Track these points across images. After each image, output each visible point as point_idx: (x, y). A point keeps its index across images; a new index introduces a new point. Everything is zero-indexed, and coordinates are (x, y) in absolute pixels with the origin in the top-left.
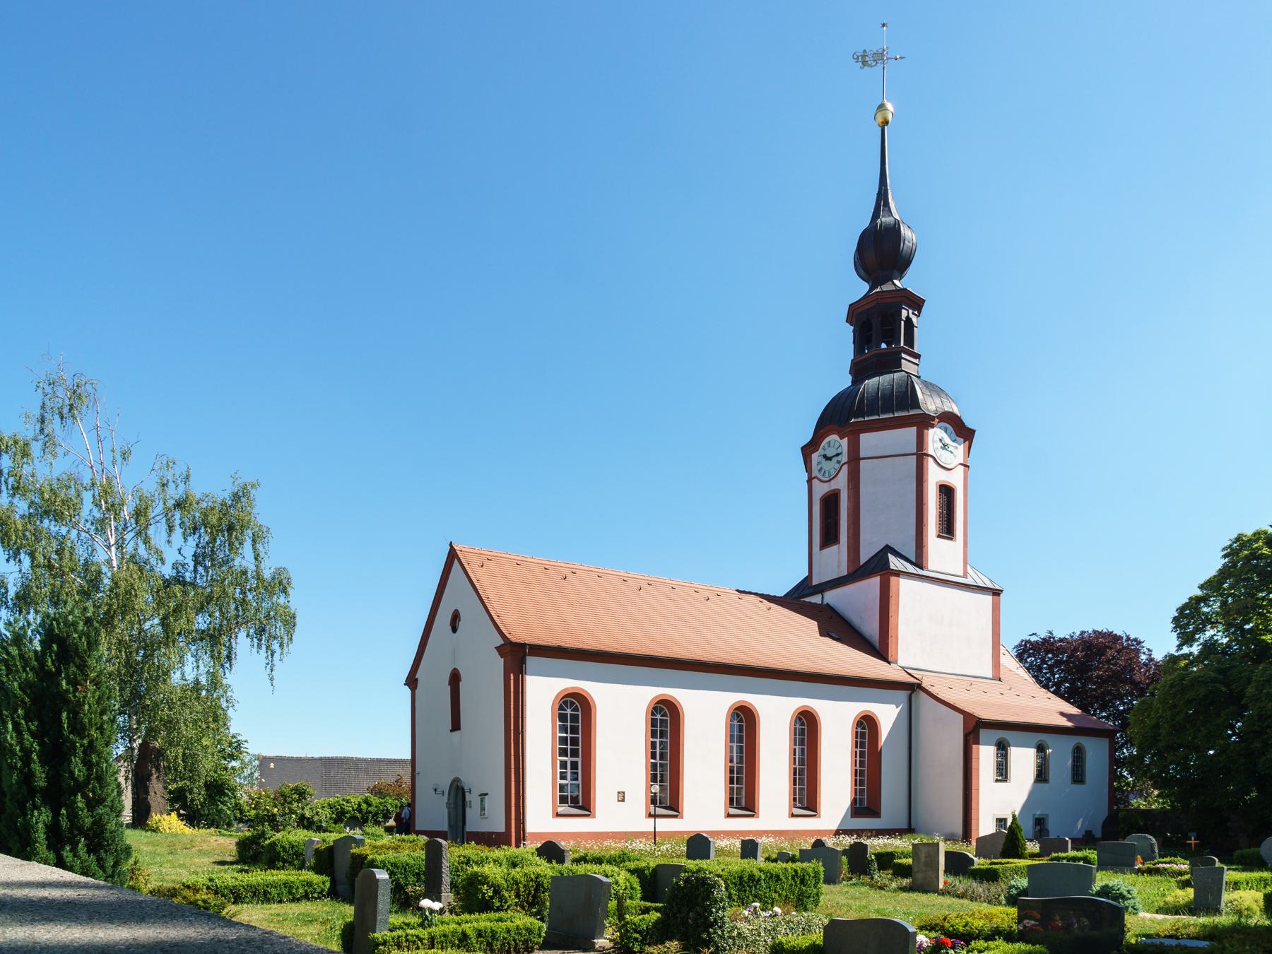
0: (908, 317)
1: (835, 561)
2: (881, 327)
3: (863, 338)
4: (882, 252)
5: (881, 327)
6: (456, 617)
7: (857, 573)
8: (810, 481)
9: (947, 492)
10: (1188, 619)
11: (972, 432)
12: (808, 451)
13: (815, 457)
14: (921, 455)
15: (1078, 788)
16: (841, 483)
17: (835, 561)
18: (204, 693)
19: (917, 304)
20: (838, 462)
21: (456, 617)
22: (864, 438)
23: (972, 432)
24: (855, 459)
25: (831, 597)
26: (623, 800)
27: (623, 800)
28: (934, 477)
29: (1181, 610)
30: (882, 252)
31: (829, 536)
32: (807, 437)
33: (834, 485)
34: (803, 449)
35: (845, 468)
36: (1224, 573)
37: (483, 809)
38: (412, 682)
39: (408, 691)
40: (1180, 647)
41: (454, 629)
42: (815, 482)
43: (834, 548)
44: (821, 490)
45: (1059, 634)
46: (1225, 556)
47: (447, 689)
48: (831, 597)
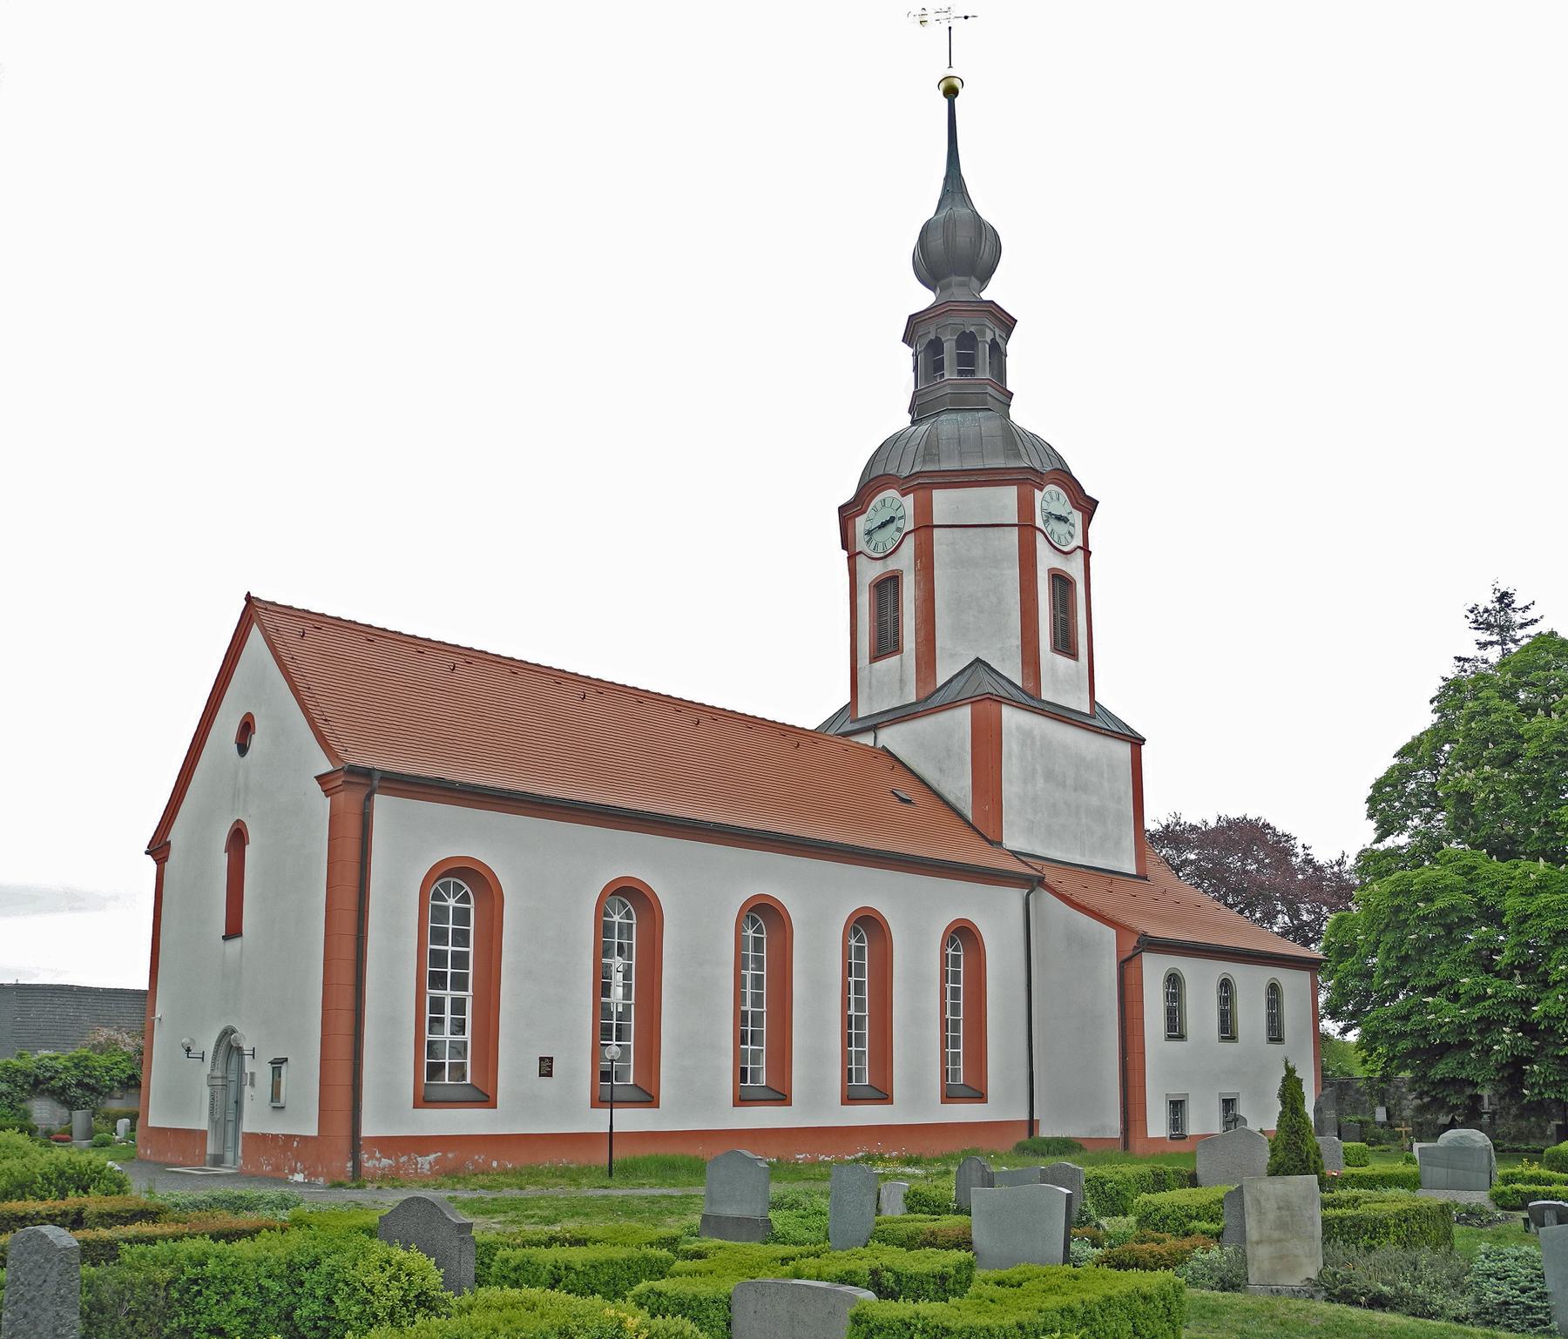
0: (993, 340)
1: (895, 680)
2: (959, 344)
3: (929, 359)
4: (957, 251)
5: (959, 344)
6: (247, 727)
7: (929, 703)
8: (852, 559)
9: (1061, 582)
10: (1387, 802)
11: (1094, 503)
12: (848, 514)
13: (861, 524)
14: (1026, 527)
15: (1176, 1045)
16: (905, 560)
17: (895, 680)
18: (1412, 786)
19: (1007, 323)
20: (899, 530)
21: (247, 727)
22: (938, 496)
23: (1094, 503)
24: (925, 527)
25: (890, 738)
26: (550, 1074)
27: (550, 1074)
28: (1046, 560)
29: (1378, 786)
30: (957, 251)
31: (885, 644)
32: (848, 492)
33: (892, 565)
34: (841, 509)
35: (910, 543)
36: (1436, 736)
37: (275, 1095)
38: (159, 849)
39: (150, 865)
40: (1379, 840)
41: (243, 748)
42: (860, 560)
43: (894, 660)
44: (870, 572)
45: (1192, 817)
46: (1434, 711)
47: (221, 861)
48: (890, 738)
